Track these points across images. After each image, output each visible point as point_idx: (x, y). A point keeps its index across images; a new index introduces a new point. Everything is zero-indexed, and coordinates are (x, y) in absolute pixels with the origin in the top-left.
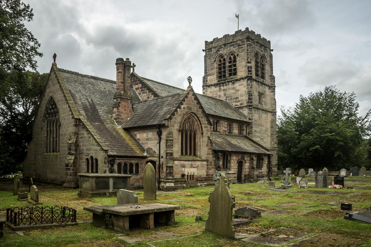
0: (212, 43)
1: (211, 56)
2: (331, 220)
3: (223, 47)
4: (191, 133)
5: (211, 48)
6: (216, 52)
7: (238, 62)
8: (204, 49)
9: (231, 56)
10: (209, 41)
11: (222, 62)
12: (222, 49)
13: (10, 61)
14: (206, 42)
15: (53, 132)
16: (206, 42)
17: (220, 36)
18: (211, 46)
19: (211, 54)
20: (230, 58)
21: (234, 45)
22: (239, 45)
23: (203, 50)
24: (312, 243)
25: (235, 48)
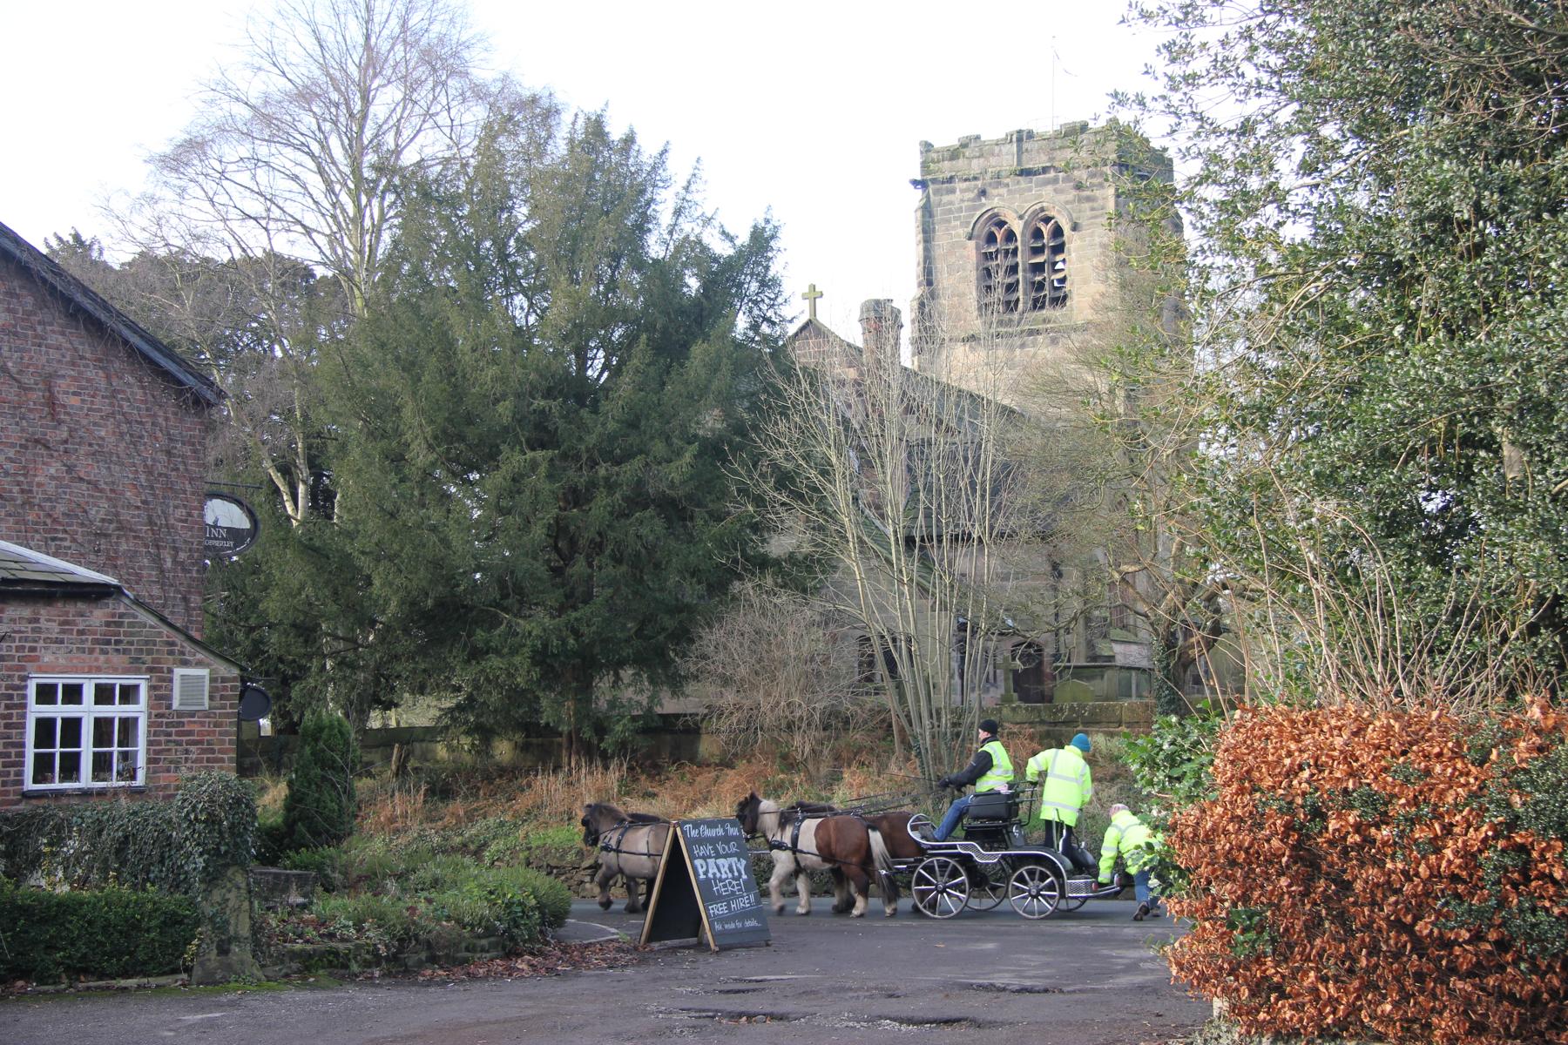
0: (954, 154)
1: (950, 211)
2: (715, 385)
3: (1008, 185)
4: (966, 450)
5: (951, 180)
6: (973, 200)
7: (1073, 255)
8: (919, 178)
9: (993, 229)
10: (937, 145)
11: (1000, 244)
12: (1003, 191)
13: (362, 187)
14: (927, 147)
15: (917, 694)
16: (927, 147)
17: (993, 130)
18: (947, 169)
19: (951, 203)
20: (1038, 234)
21: (1055, 180)
22: (1079, 187)
23: (915, 183)
24: (957, 539)
25: (1062, 198)
